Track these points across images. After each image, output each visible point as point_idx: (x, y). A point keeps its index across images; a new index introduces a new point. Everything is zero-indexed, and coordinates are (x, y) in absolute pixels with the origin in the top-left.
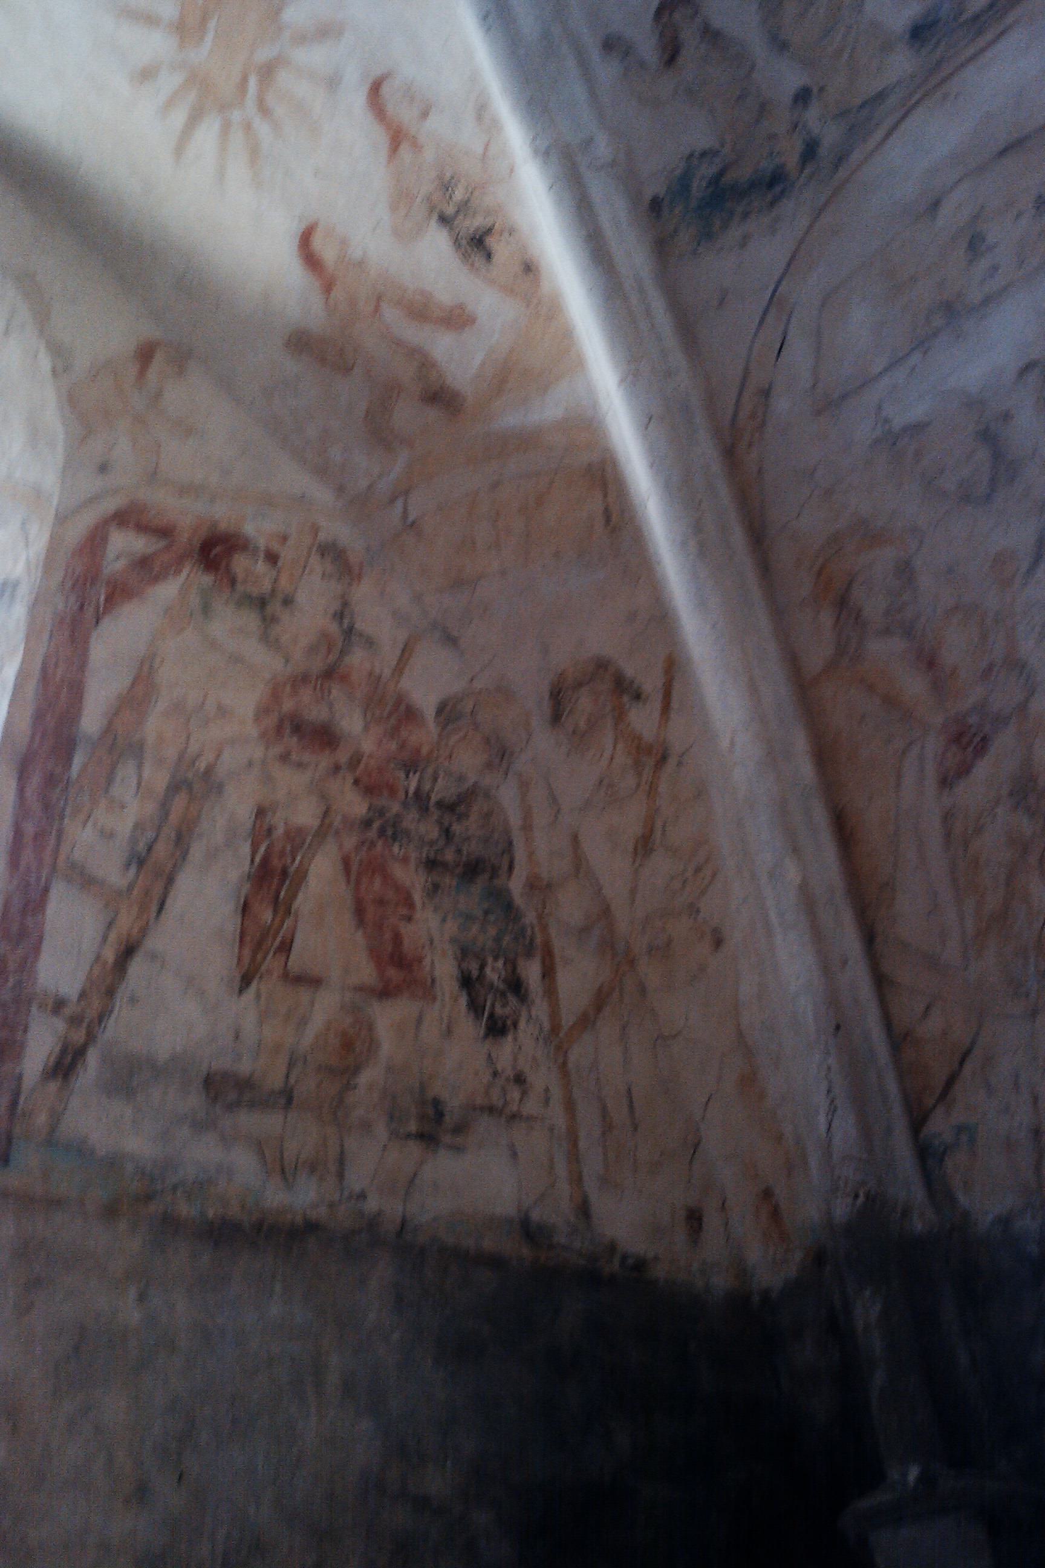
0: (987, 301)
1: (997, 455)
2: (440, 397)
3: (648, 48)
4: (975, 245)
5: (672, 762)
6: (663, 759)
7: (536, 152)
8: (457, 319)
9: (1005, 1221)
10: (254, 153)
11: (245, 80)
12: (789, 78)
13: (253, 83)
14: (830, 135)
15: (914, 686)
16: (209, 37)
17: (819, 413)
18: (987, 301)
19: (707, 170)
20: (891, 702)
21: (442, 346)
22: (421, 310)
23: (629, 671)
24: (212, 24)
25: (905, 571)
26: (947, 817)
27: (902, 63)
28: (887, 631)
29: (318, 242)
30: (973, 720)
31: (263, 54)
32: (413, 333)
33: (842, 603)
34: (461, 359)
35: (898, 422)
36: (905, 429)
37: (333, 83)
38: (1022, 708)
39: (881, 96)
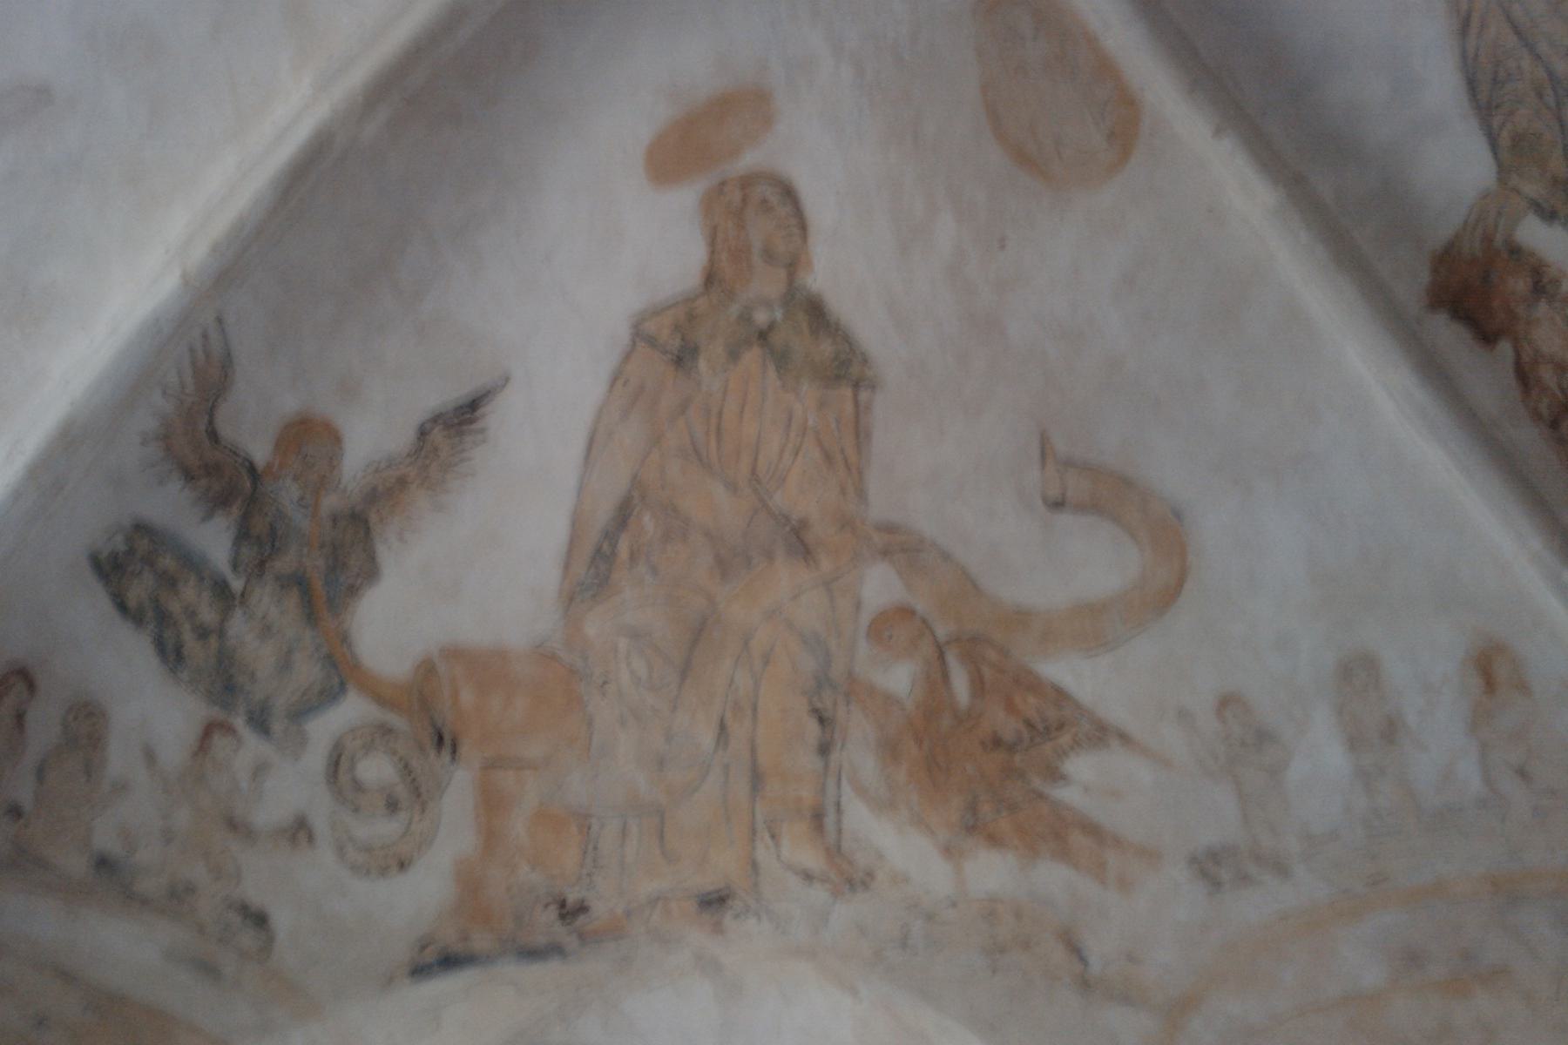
27: (76, 864)
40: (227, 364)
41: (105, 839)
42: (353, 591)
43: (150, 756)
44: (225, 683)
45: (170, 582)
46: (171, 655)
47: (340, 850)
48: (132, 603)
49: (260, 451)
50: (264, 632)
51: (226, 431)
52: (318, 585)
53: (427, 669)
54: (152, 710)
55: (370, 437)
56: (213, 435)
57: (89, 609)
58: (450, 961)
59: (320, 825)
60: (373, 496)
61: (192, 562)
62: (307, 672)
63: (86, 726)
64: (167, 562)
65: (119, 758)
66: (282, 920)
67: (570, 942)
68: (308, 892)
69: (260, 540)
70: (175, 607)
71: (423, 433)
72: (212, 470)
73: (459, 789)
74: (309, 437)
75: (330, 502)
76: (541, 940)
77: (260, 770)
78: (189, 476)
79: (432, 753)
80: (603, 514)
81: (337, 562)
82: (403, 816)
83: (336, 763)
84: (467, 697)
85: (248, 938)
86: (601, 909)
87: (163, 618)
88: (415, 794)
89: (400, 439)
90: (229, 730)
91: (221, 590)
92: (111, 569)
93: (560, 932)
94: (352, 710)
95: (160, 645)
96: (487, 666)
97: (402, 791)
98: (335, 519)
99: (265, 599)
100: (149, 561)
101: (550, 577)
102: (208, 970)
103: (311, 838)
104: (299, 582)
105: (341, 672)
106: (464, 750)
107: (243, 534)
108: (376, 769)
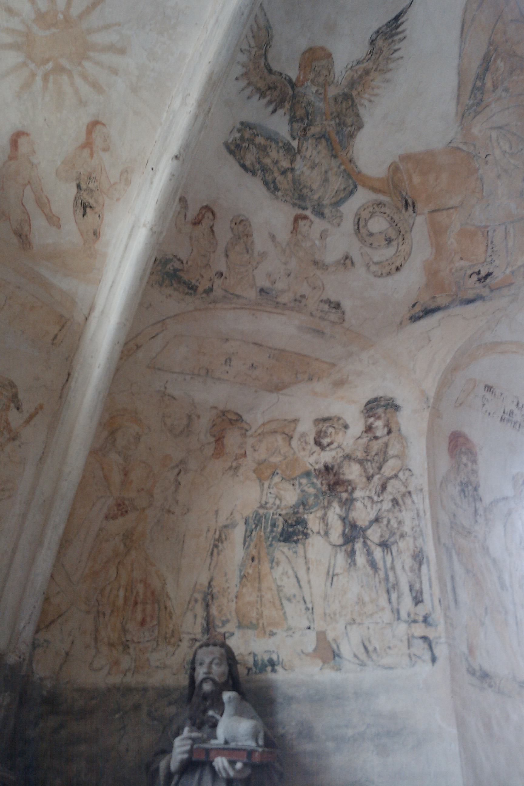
0: (219, 379)
1: (188, 426)
2: (23, 237)
3: (192, 214)
4: (228, 361)
5: (17, 443)
6: (14, 439)
7: (151, 229)
8: (54, 221)
9: (41, 679)
10: (27, 86)
11: (48, 61)
12: (221, 265)
13: (50, 65)
14: (218, 292)
15: (116, 477)
16: (48, 33)
17: (148, 367)
18: (219, 379)
19: (177, 265)
20: (106, 477)
21: (39, 222)
22: (42, 203)
23: (20, 397)
24: (54, 30)
25: (138, 438)
26: (101, 530)
27: (252, 294)
28: (119, 453)
29: (22, 141)
30: (127, 502)
31: (64, 62)
32: (31, 206)
33: (112, 433)
34: (41, 233)
35: (169, 391)
36: (169, 395)
37: (82, 103)
38: (144, 509)
39: (238, 297)
40: (268, 28)
41: (262, 282)
42: (352, 136)
43: (273, 237)
44: (299, 196)
45: (263, 149)
46: (272, 187)
47: (368, 266)
48: (248, 163)
49: (293, 74)
50: (313, 166)
51: (275, 67)
52: (333, 135)
53: (394, 169)
54: (270, 215)
55: (346, 52)
56: (270, 71)
57: (230, 170)
58: (428, 312)
59: (357, 258)
60: (352, 84)
61: (272, 138)
62: (337, 183)
63: (242, 228)
64: (259, 140)
65: (260, 242)
66: (347, 305)
67: (485, 292)
68: (354, 289)
69: (302, 119)
70: (268, 161)
71: (372, 42)
72: (271, 88)
73: (420, 224)
74: (315, 58)
75: (332, 92)
76: (470, 294)
77: (323, 236)
78: (263, 95)
79: (404, 211)
80: (474, 67)
81: (341, 124)
82: (394, 243)
83: (359, 224)
84: (416, 180)
85: (333, 316)
86: (499, 275)
87: (265, 169)
88: (398, 234)
89: (361, 50)
90: (305, 218)
91: (288, 148)
92: (235, 149)
93: (479, 289)
94: (362, 197)
95: (266, 183)
96: (422, 162)
97: (392, 234)
98: (335, 99)
99: (312, 151)
100: (251, 141)
101: (449, 106)
102: (320, 333)
103: (352, 263)
104: (323, 136)
105: (353, 179)
106: (419, 206)
107: (293, 120)
108: (378, 225)
